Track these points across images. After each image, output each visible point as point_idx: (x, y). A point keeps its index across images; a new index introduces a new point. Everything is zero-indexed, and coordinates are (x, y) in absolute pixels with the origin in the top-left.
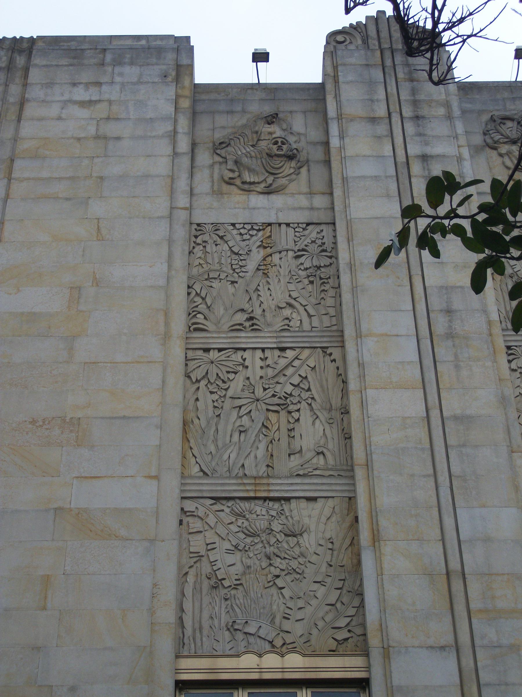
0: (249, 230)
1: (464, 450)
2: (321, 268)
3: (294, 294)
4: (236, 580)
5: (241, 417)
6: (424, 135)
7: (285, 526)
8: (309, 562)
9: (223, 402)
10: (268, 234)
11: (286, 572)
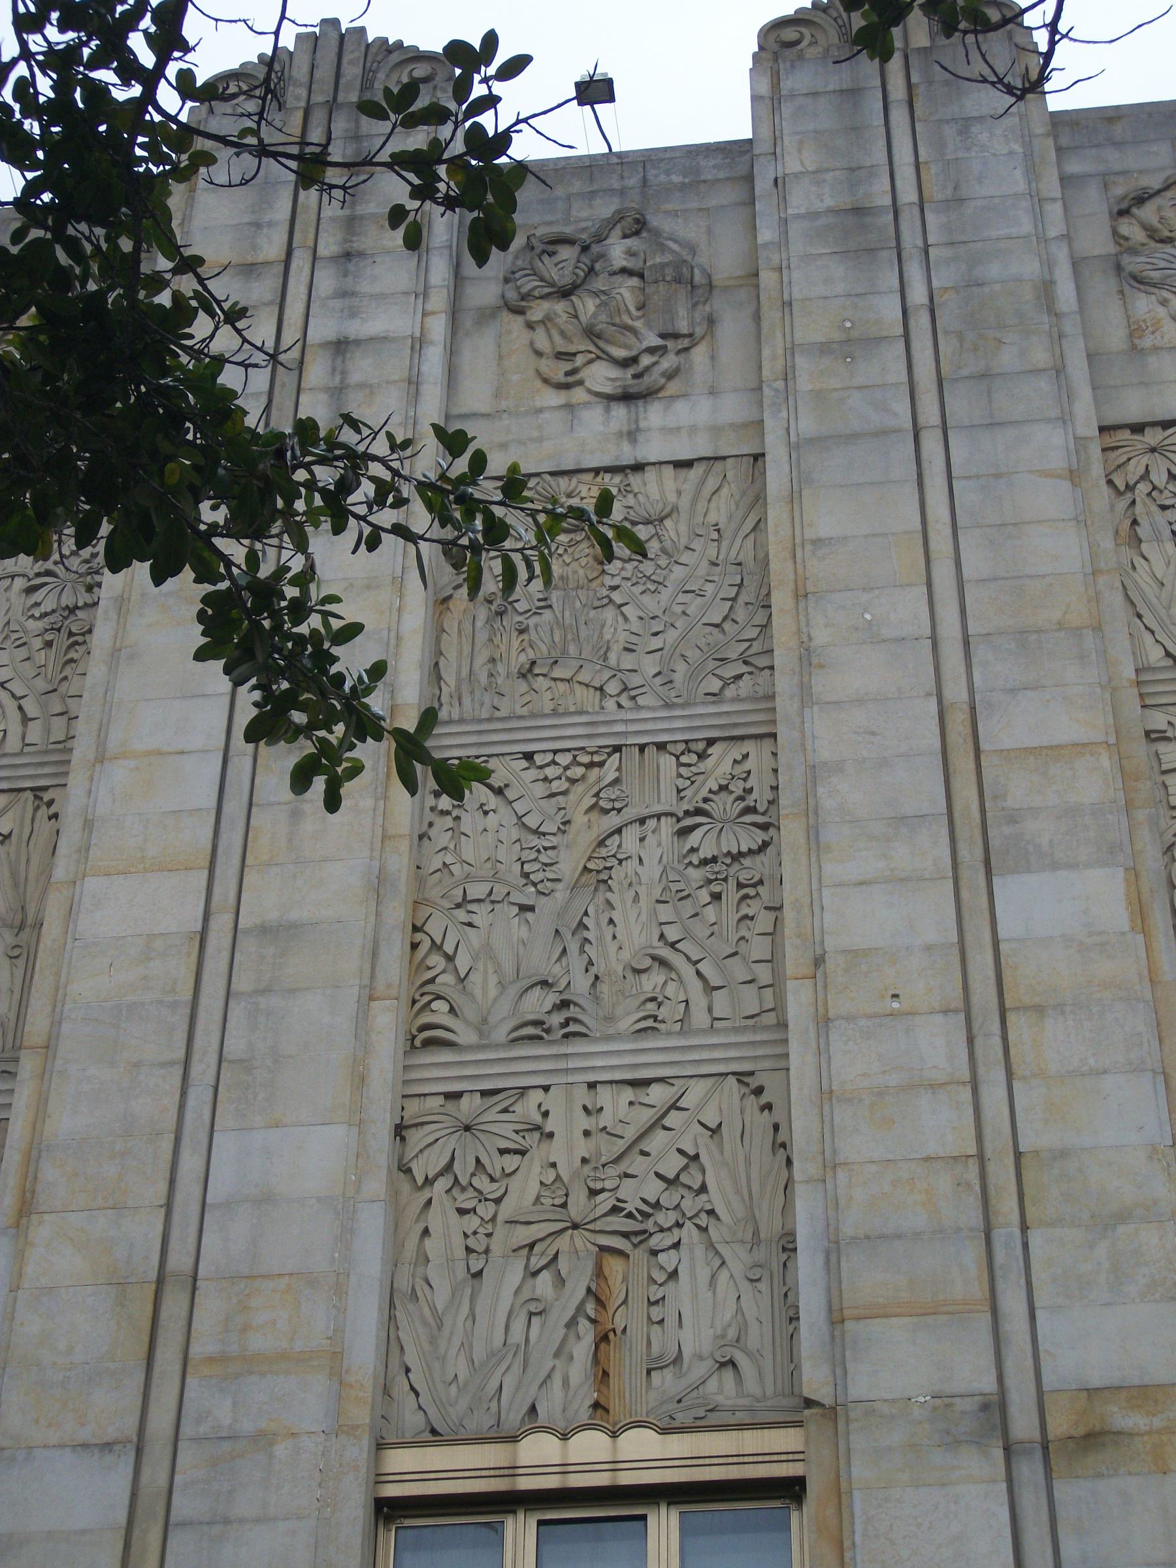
0: (566, 768)
1: (263, 1002)
2: (742, 860)
3: (672, 934)
4: (539, 600)
5: (535, 1274)
6: (353, 294)
9: (489, 1235)
10: (612, 775)
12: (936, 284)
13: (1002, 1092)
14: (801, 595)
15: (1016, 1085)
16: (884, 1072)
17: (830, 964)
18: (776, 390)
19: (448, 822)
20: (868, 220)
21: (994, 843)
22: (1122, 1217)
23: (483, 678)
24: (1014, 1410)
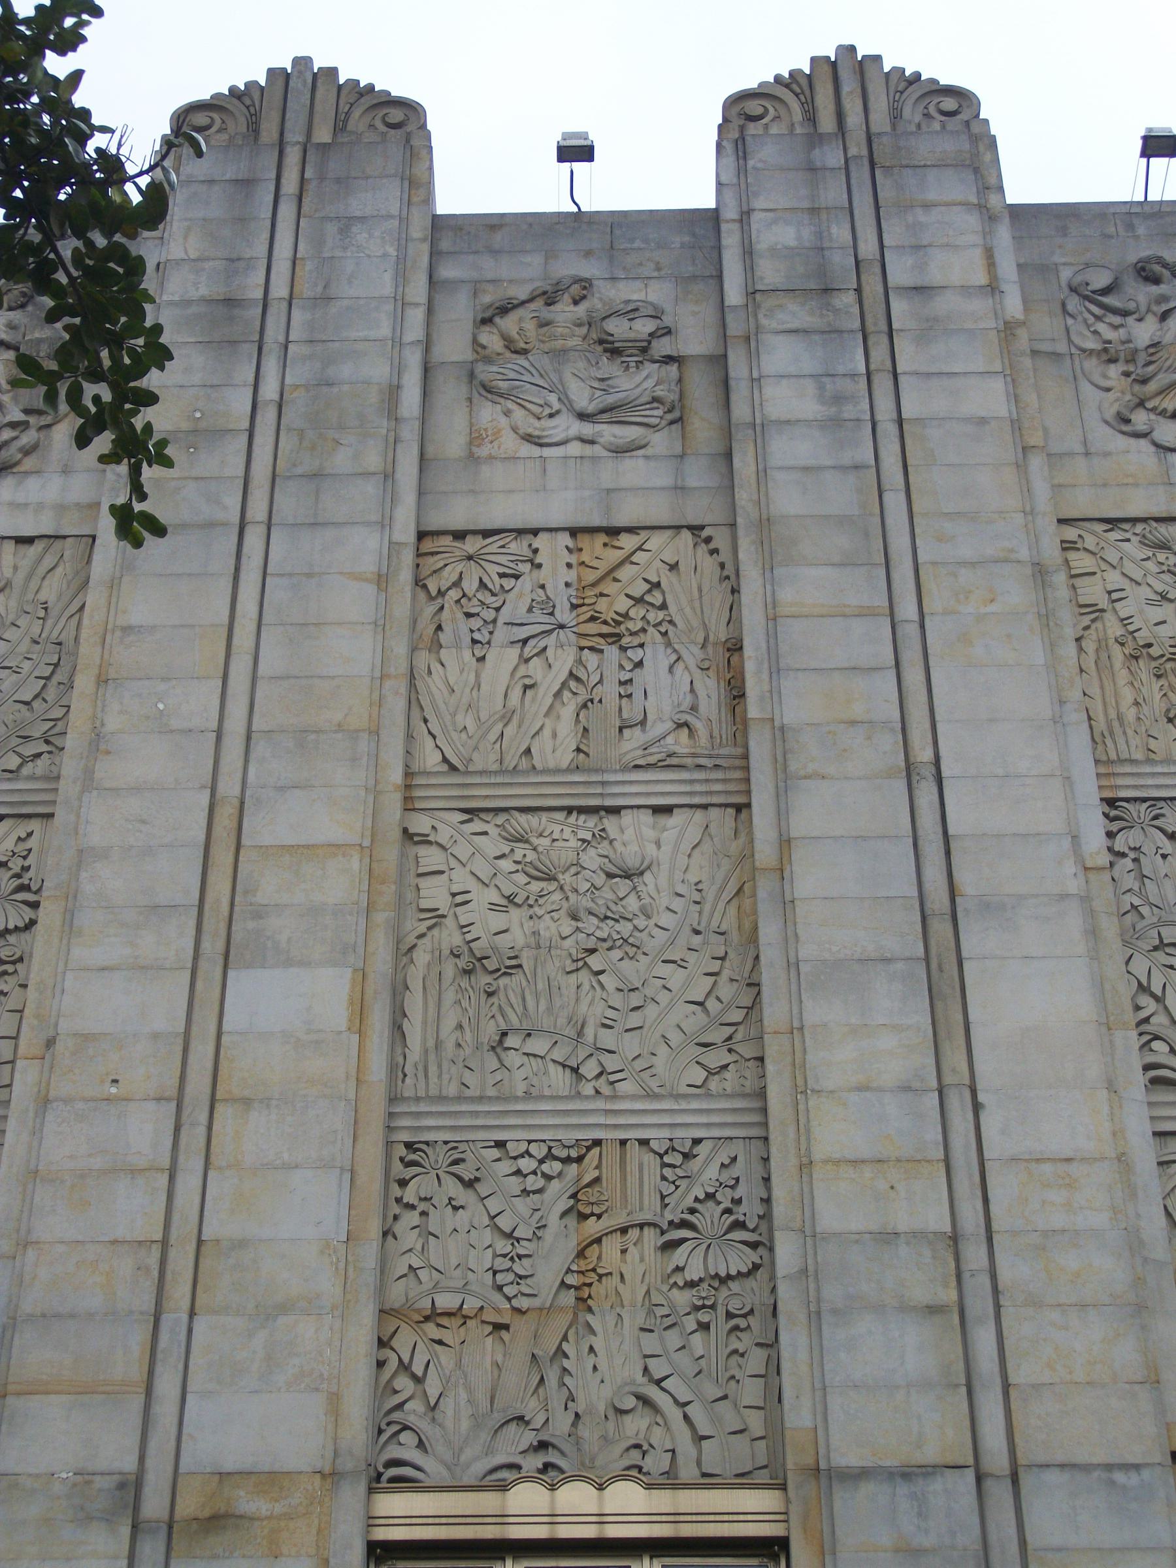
2: (730, 1283)
3: (658, 1368)
4: (510, 958)
5: (527, 661)
8: (656, 925)
12: (288, 381)
13: (197, 1181)
14: (102, 681)
15: (211, 1174)
16: (90, 1155)
17: (59, 1046)
18: (119, 475)
19: (413, 1218)
20: (236, 311)
21: (237, 937)
22: (284, 1308)
23: (450, 1045)
24: (148, 1491)
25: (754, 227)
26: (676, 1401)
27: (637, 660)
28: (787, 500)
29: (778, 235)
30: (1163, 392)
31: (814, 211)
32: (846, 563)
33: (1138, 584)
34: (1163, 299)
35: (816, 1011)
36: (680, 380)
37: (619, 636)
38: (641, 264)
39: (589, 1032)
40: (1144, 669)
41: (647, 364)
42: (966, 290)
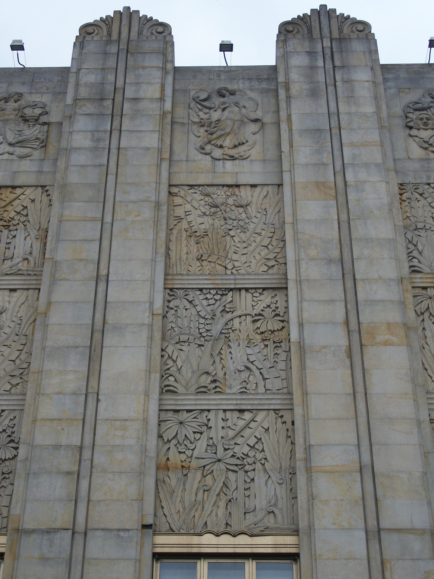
2: (275, 332)
7: (235, 202)
10: (230, 299)
11: (237, 228)
25: (81, 75)
26: (257, 367)
27: (14, 235)
28: (74, 178)
29: (89, 78)
30: (218, 138)
31: (103, 69)
32: (90, 201)
33: (196, 209)
34: (224, 103)
35: (49, 365)
36: (48, 131)
37: (9, 226)
38: (42, 88)
39: (229, 255)
40: (192, 241)
41: (37, 125)
42: (151, 100)
